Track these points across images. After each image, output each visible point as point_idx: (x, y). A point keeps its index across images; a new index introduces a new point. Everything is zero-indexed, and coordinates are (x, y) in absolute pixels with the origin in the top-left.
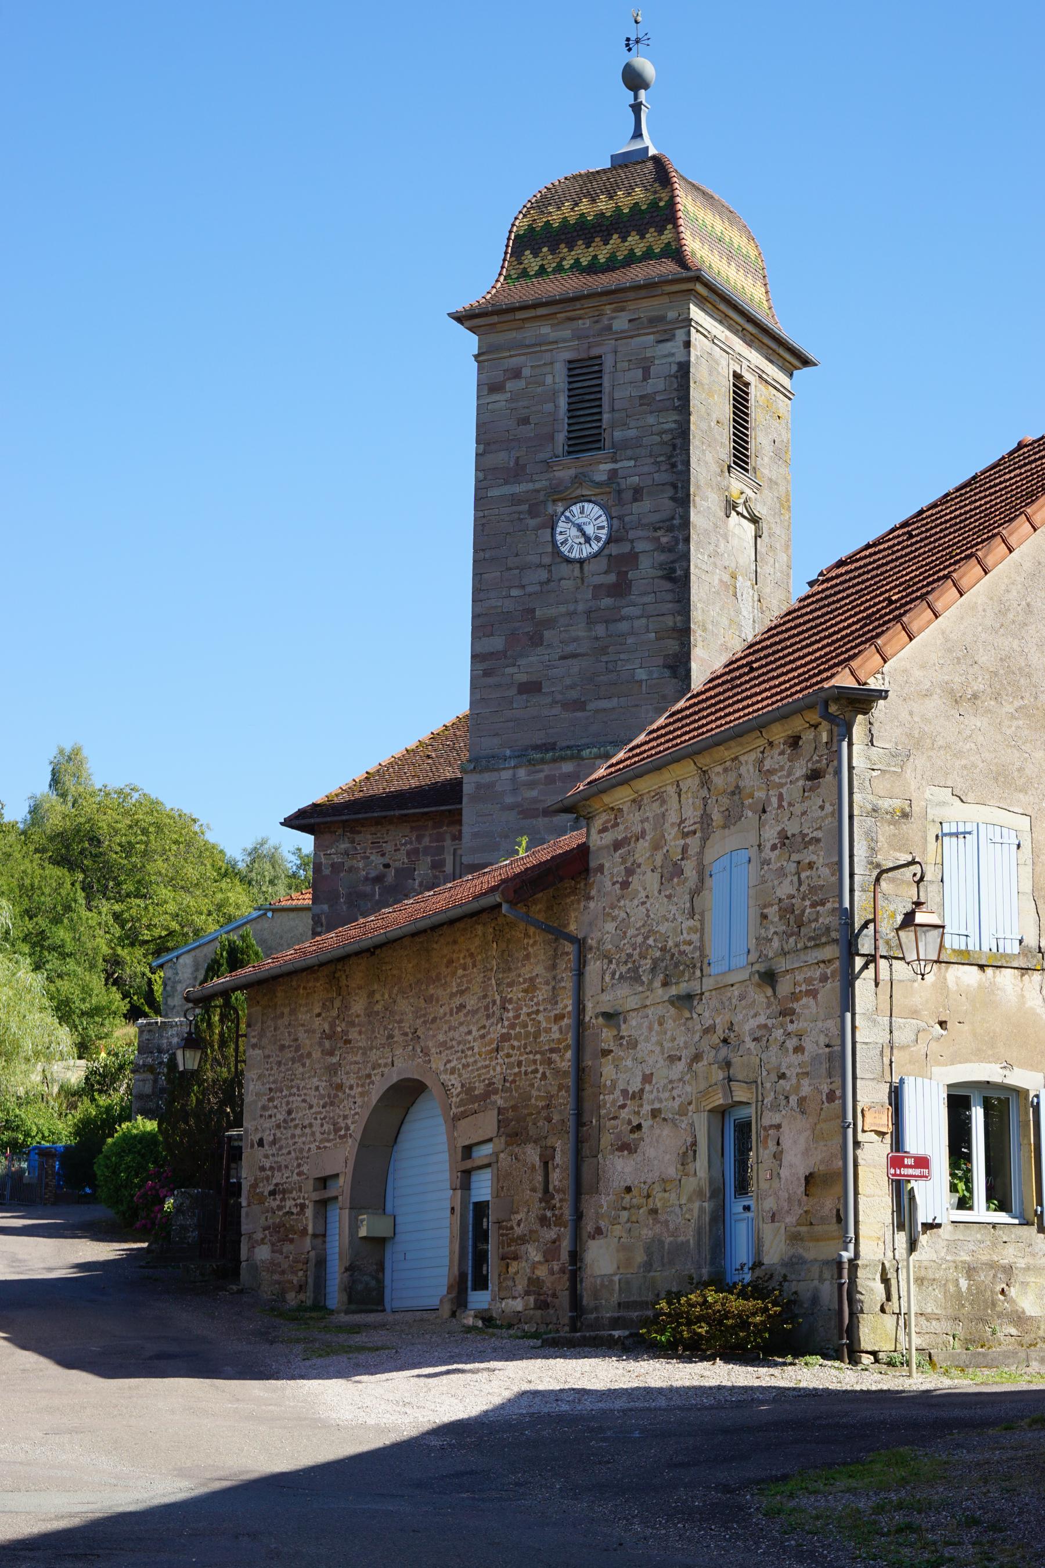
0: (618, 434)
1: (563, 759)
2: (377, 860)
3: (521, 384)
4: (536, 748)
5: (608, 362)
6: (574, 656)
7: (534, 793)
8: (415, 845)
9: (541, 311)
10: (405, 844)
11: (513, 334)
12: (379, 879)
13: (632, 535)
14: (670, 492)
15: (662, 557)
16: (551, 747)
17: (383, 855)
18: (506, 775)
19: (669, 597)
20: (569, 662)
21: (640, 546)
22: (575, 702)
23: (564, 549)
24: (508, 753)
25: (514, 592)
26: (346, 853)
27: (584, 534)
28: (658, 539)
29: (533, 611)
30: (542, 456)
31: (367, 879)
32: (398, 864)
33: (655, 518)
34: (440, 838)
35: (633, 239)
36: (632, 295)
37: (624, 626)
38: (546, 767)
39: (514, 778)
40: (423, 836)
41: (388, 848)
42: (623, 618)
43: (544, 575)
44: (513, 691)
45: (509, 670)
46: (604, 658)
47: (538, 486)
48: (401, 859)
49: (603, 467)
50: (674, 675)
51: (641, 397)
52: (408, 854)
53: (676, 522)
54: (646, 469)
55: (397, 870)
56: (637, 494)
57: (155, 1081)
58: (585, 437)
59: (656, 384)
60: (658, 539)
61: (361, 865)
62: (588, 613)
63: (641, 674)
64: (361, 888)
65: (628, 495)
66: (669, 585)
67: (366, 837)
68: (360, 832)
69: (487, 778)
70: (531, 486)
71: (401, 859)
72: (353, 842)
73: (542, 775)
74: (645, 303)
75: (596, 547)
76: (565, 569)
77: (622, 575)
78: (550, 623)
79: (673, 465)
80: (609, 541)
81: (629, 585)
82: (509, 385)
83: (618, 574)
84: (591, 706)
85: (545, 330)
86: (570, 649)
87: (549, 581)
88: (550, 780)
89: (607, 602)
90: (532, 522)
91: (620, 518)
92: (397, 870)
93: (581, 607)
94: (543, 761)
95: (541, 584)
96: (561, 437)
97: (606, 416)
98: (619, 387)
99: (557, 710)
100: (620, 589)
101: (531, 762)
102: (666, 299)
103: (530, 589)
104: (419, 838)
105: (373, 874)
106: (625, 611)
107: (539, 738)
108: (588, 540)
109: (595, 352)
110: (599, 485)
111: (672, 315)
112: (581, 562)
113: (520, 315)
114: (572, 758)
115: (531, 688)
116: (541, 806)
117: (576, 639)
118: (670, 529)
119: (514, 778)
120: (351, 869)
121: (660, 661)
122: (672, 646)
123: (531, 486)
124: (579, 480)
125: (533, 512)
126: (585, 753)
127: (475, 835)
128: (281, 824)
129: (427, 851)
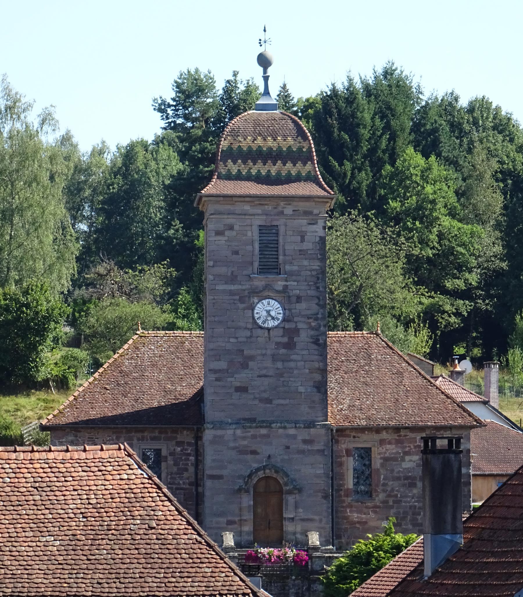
0: (288, 268)
1: (261, 427)
3: (234, 233)
4: (245, 419)
5: (282, 230)
6: (266, 376)
7: (245, 443)
13: (296, 319)
15: (312, 333)
16: (252, 420)
18: (230, 432)
19: (316, 353)
20: (263, 379)
21: (300, 326)
23: (260, 322)
24: (230, 421)
25: (232, 340)
30: (245, 272)
33: (309, 312)
35: (289, 165)
37: (292, 364)
43: (248, 334)
44: (232, 390)
46: (282, 379)
47: (244, 287)
49: (280, 283)
51: (300, 251)
54: (303, 288)
56: (299, 299)
62: (273, 356)
63: (301, 389)
65: (294, 299)
66: (316, 347)
69: (219, 432)
70: (240, 287)
72: (76, 436)
75: (276, 323)
77: (291, 339)
78: (252, 358)
80: (284, 320)
81: (295, 344)
82: (227, 233)
83: (289, 338)
84: (276, 402)
86: (264, 372)
87: (251, 337)
88: (254, 437)
89: (283, 351)
90: (242, 306)
91: (290, 310)
93: (269, 352)
94: (250, 427)
95: (247, 338)
96: (256, 264)
97: (281, 258)
99: (257, 402)
100: (290, 345)
102: (314, 203)
103: (240, 339)
106: (294, 357)
107: (247, 415)
109: (275, 223)
110: (278, 292)
112: (269, 329)
114: (266, 427)
115: (242, 389)
116: (249, 449)
121: (312, 384)
122: (318, 377)
123: (240, 287)
124: (267, 287)
125: (242, 300)
127: (214, 461)
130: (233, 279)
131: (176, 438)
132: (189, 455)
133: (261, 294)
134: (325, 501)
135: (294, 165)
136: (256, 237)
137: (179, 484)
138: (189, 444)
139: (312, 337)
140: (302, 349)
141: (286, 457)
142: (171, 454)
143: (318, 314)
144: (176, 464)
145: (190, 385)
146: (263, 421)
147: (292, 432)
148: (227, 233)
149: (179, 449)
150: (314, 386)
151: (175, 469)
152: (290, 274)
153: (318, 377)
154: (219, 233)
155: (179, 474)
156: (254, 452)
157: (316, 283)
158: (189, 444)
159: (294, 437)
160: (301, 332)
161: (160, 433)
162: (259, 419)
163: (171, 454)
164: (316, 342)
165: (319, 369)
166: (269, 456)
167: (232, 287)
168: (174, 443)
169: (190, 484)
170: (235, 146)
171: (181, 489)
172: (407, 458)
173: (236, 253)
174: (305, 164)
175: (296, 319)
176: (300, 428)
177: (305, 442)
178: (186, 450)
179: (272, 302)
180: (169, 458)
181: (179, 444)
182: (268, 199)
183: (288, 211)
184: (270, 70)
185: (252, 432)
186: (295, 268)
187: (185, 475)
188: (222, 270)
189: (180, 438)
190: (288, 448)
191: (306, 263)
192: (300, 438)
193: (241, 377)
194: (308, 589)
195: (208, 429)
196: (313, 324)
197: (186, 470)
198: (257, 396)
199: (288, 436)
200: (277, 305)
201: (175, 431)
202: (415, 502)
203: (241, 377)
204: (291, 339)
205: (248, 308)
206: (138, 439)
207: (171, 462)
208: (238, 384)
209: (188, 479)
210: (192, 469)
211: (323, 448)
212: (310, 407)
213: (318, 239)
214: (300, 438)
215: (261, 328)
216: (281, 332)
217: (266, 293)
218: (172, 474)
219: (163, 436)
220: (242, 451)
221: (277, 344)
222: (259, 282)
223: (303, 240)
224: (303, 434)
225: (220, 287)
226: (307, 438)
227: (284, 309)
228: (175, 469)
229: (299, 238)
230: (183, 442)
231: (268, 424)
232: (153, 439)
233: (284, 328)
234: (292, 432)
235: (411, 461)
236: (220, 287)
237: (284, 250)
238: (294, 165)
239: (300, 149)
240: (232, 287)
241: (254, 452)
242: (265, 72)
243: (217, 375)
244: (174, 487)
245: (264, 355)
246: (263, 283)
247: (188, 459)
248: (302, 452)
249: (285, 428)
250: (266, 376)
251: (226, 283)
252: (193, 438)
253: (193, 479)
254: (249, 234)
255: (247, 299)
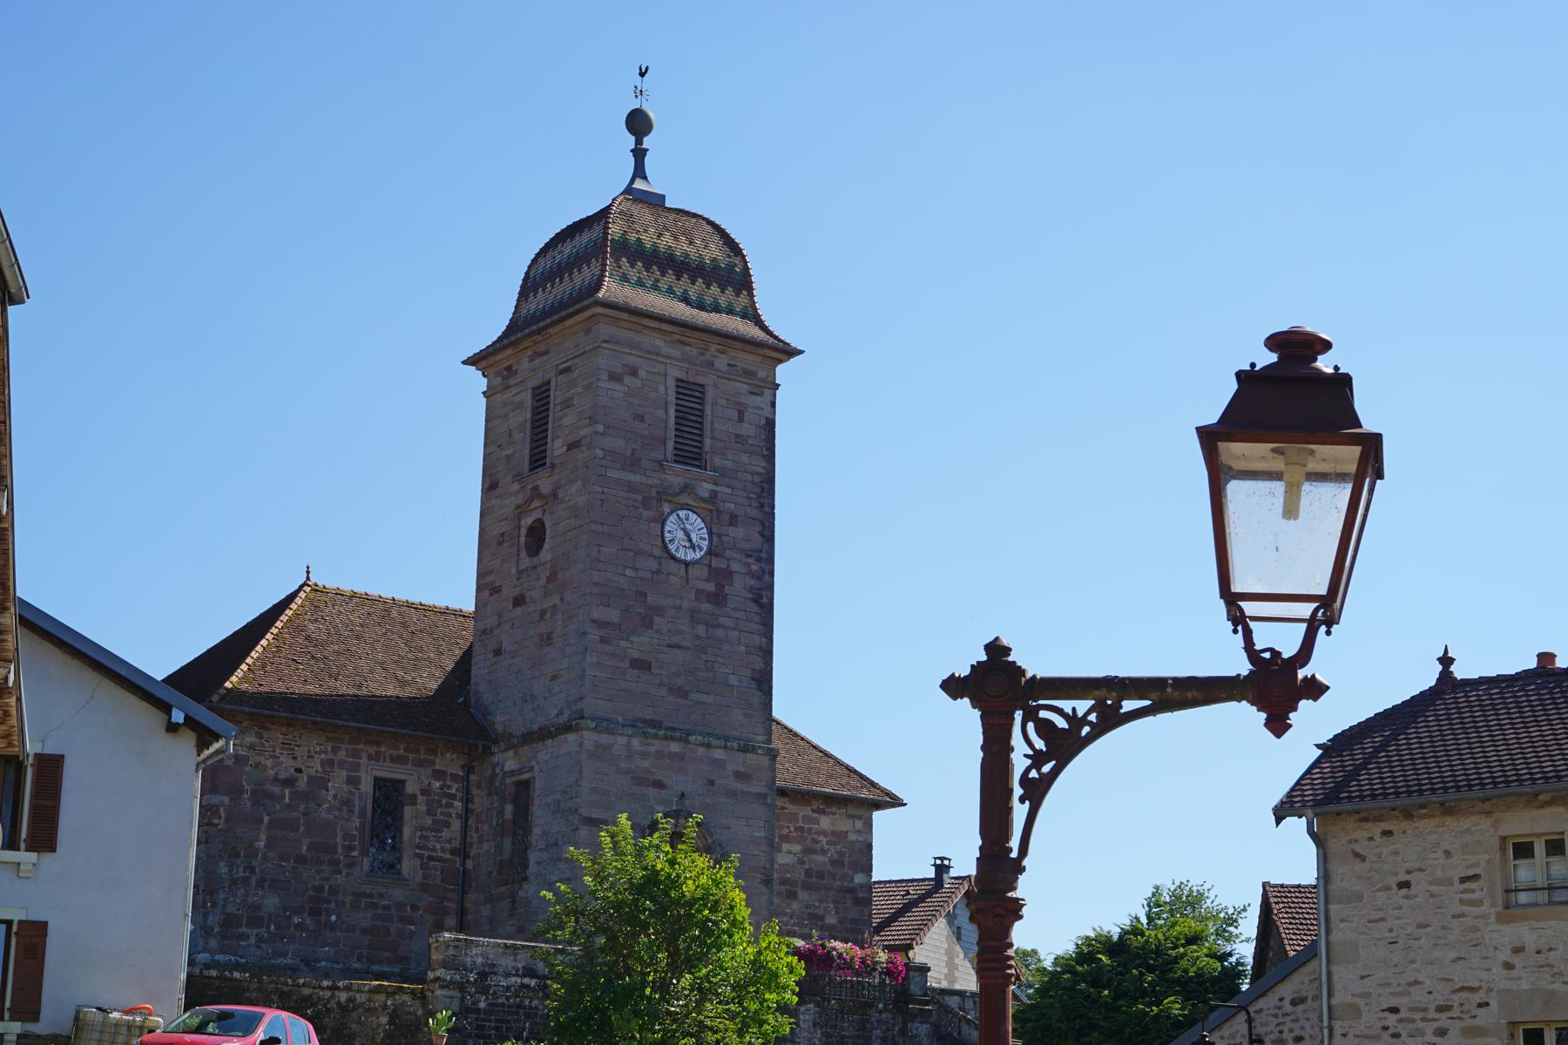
0: (718, 461)
1: (673, 739)
2: (285, 759)
3: (638, 383)
4: (644, 721)
5: (710, 394)
6: (680, 647)
7: (646, 764)
8: (330, 756)
9: (665, 326)
10: (320, 752)
11: (631, 335)
12: (290, 782)
13: (728, 553)
14: (758, 528)
15: (752, 582)
16: (657, 724)
17: (295, 758)
18: (622, 740)
19: (757, 619)
20: (676, 651)
21: (735, 567)
22: (679, 689)
23: (672, 547)
24: (620, 720)
25: (629, 572)
26: (252, 747)
27: (690, 540)
28: (749, 565)
29: (645, 595)
30: (654, 455)
31: (276, 779)
32: (312, 772)
33: (748, 546)
34: (356, 754)
35: (715, 289)
36: (739, 345)
37: (720, 633)
38: (656, 742)
39: (628, 746)
40: (339, 749)
41: (300, 752)
42: (720, 626)
43: (655, 566)
44: (626, 664)
45: (623, 643)
46: (704, 657)
47: (650, 482)
48: (315, 768)
49: (705, 485)
50: (760, 688)
51: (737, 436)
52: (323, 763)
53: (764, 555)
54: (740, 500)
55: (310, 778)
56: (733, 520)
57: (462, 999)
58: (690, 454)
59: (747, 429)
60: (749, 565)
61: (269, 763)
62: (692, 612)
63: (733, 680)
64: (269, 787)
65: (726, 518)
66: (756, 609)
67: (276, 736)
68: (268, 729)
69: (605, 739)
70: (644, 480)
71: (315, 768)
72: (261, 737)
73: (653, 749)
74: (742, 355)
75: (698, 555)
76: (672, 566)
77: (720, 587)
78: (660, 611)
79: (762, 505)
80: (710, 552)
81: (725, 598)
82: (627, 379)
83: (717, 585)
84: (693, 696)
85: (659, 343)
86: (676, 640)
87: (658, 572)
88: (660, 755)
89: (707, 607)
90: (646, 514)
91: (719, 536)
92: (310, 778)
93: (685, 605)
94: (656, 737)
95: (652, 573)
96: (670, 445)
97: (708, 442)
98: (718, 421)
99: (663, 692)
100: (718, 598)
101: (645, 735)
102: (759, 359)
103: (641, 574)
104: (335, 750)
105: (283, 776)
106: (723, 620)
107: (648, 714)
108: (693, 547)
109: (700, 380)
110: (704, 500)
111: (761, 374)
112: (687, 564)
113: (646, 322)
114: (680, 740)
115: (641, 665)
116: (651, 777)
117: (681, 632)
118: (758, 560)
119: (628, 746)
120: (257, 765)
121: (749, 673)
122: (759, 663)
123: (644, 480)
124: (686, 488)
125: (645, 503)
126: (692, 738)
127: (593, 791)
128: (895, 802)
129: (342, 764)
130: (633, 463)
131: (433, 763)
132: (453, 797)
133: (675, 498)
134: (764, 889)
135: (723, 291)
136: (672, 398)
137: (434, 849)
138: (454, 777)
139: (751, 589)
140: (738, 610)
141: (708, 801)
142: (424, 792)
143: (760, 551)
144: (430, 812)
145: (432, 676)
146: (673, 729)
147: (719, 754)
148: (627, 379)
149: (437, 784)
150: (753, 679)
151: (429, 821)
152: (723, 472)
153: (759, 663)
154: (614, 377)
155: (435, 830)
156: (659, 785)
157: (760, 497)
158: (454, 777)
159: (721, 764)
160: (736, 578)
161: (407, 750)
162: (666, 723)
163: (424, 792)
164: (757, 600)
165: (760, 648)
166: (683, 795)
167: (635, 478)
168: (429, 771)
169: (453, 852)
170: (632, 237)
171: (439, 859)
172: (785, 847)
173: (641, 418)
174: (738, 294)
175: (728, 553)
176: (732, 748)
177: (739, 776)
178: (450, 787)
179: (693, 517)
180: (420, 798)
181: (439, 775)
182: (697, 334)
183: (721, 362)
184: (647, 142)
185: (656, 746)
186: (729, 464)
187: (445, 834)
188: (617, 444)
189: (439, 765)
190: (712, 783)
191: (745, 458)
192: (730, 767)
193: (640, 644)
194: (903, 1032)
195: (588, 728)
196: (754, 568)
197: (448, 825)
198: (665, 681)
199: (713, 762)
200: (699, 523)
201: (433, 752)
202: (795, 924)
203: (640, 644)
204: (720, 587)
205: (654, 520)
206: (370, 758)
207: (422, 807)
208: (636, 655)
209: (449, 841)
210: (456, 825)
211: (763, 790)
212: (746, 715)
213: (763, 422)
214: (730, 767)
215: (673, 558)
216: (705, 572)
217: (684, 499)
218: (422, 829)
219: (411, 756)
220: (639, 781)
221: (699, 591)
222: (676, 476)
223: (741, 418)
224: (736, 762)
225: (613, 474)
226: (742, 769)
227: (710, 533)
228: (429, 821)
229: (735, 414)
230: (443, 773)
231: (672, 734)
232: (396, 759)
233: (710, 566)
234: (719, 754)
235: (790, 852)
236: (613, 474)
237: (713, 430)
238: (723, 291)
239: (731, 266)
240: (635, 478)
241: (659, 785)
242: (639, 142)
243: (602, 633)
244: (426, 853)
245: (679, 608)
246: (680, 480)
247: (450, 805)
248: (732, 794)
249: (709, 746)
250: (680, 647)
251: (623, 469)
252: (463, 767)
253: (456, 844)
254: (662, 389)
255: (654, 503)
